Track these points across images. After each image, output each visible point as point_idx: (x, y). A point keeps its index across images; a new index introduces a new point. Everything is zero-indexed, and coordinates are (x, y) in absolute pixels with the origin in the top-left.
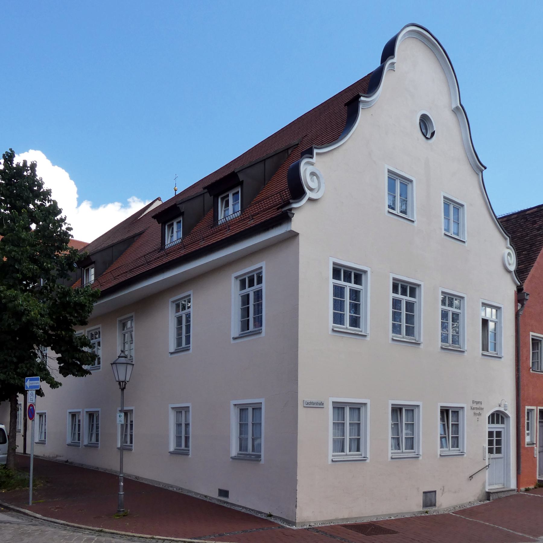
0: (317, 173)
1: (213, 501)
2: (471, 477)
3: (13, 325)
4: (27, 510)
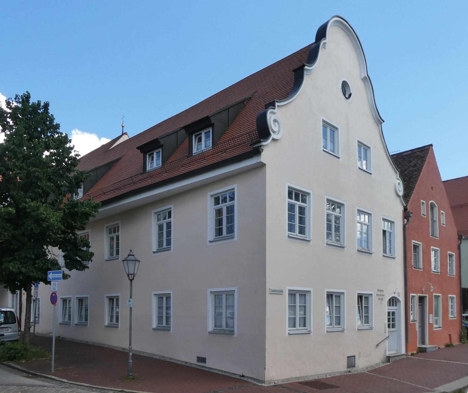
0: (278, 120)
1: (193, 366)
2: (378, 345)
3: (35, 229)
4: (53, 376)
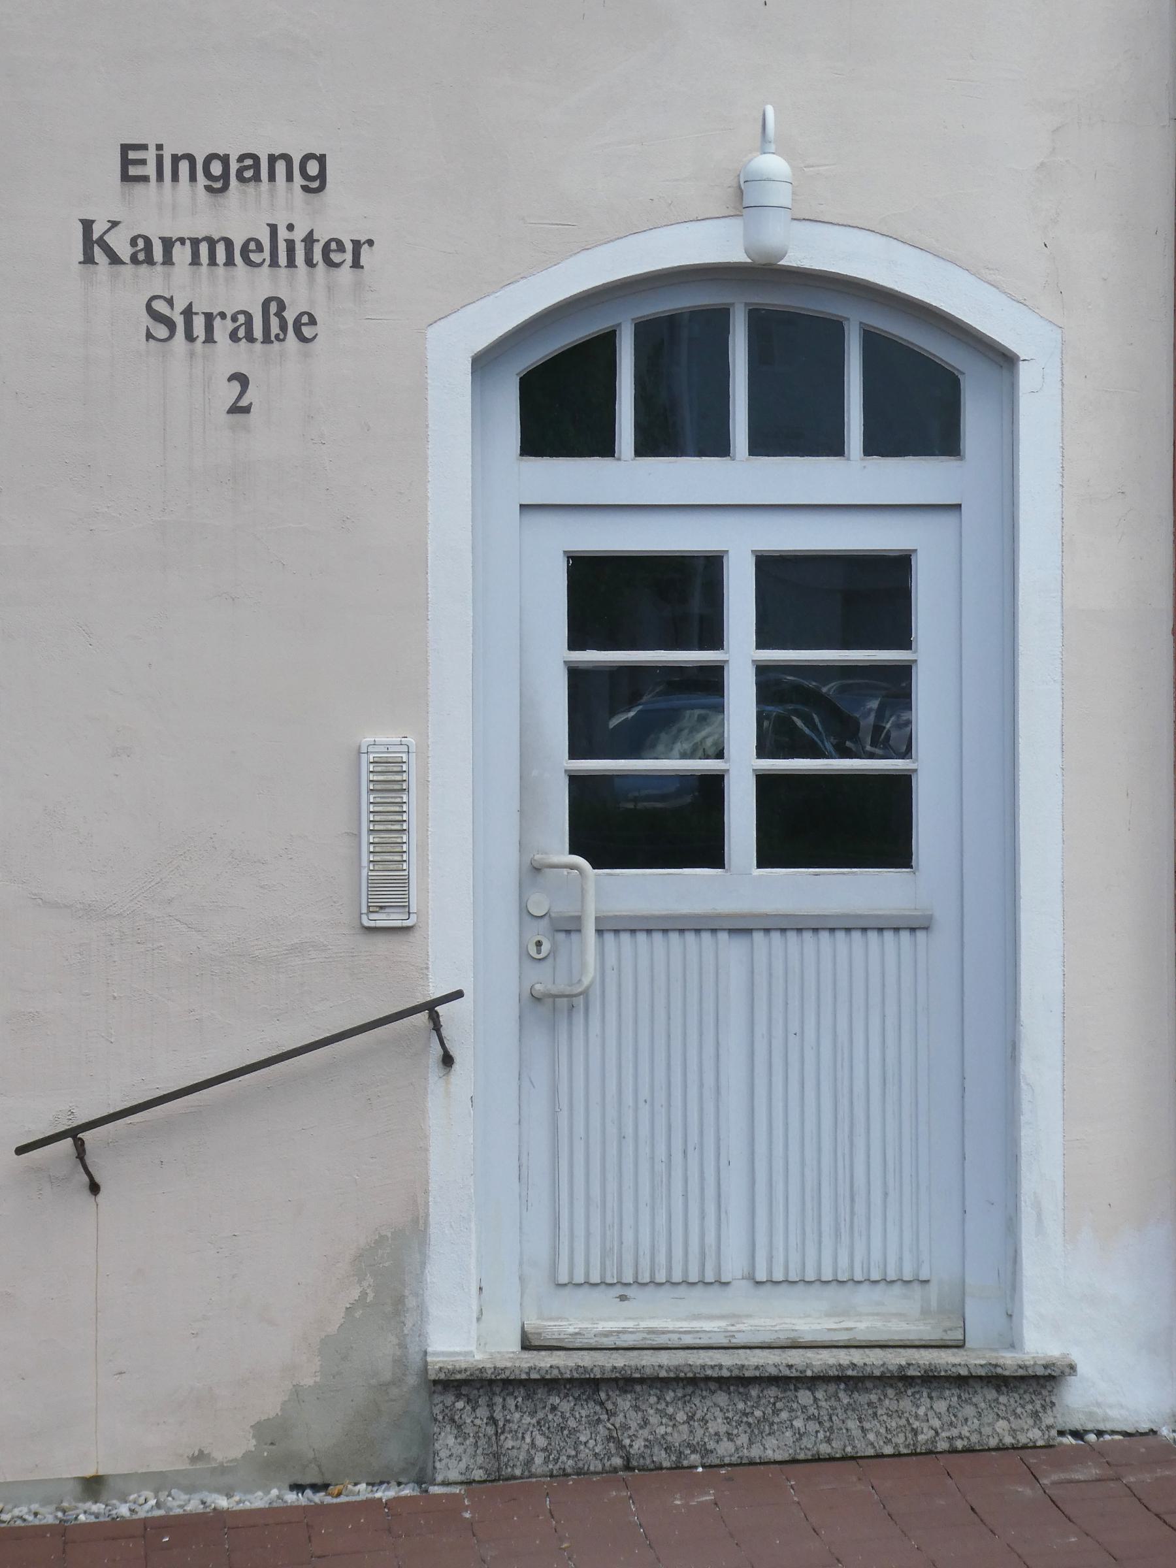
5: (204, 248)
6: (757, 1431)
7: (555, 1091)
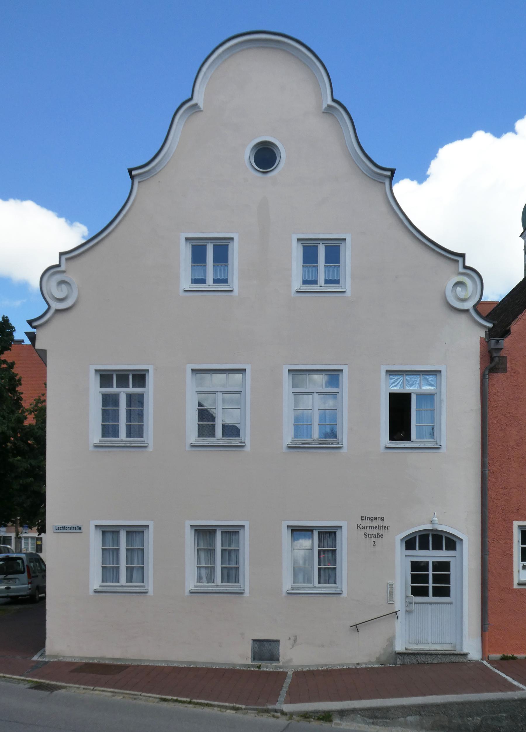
2: (356, 627)
5: (370, 527)
6: (433, 660)
7: (409, 621)
